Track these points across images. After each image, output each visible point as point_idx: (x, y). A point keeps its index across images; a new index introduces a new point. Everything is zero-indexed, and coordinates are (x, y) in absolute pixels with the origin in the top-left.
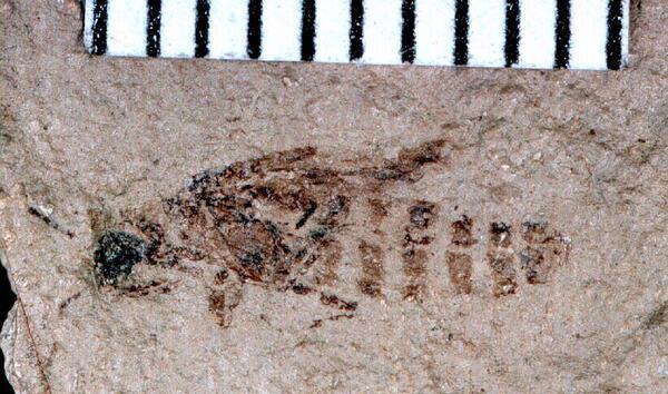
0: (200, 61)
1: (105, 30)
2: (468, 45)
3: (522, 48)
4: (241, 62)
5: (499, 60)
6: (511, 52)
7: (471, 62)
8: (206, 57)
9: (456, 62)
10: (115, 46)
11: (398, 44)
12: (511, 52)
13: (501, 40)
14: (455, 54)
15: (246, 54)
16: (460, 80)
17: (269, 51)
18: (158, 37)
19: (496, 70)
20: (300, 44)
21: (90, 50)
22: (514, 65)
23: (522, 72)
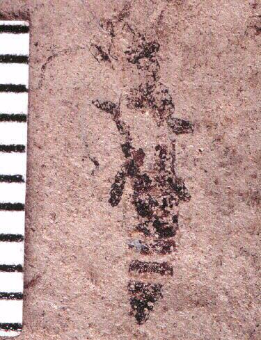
0: (32, 60)
1: (7, 324)
2: (15, 114)
3: (17, 83)
4: (31, 36)
5: (24, 96)
6: (19, 89)
7: (25, 112)
8: (23, 266)
9: (25, 121)
10: (18, 318)
11: (15, 213)
12: (19, 89)
13: (12, 95)
14: (20, 122)
15: (21, 243)
16: (25, 328)
17: (22, 171)
18: (12, 294)
19: (29, 97)
20: (18, 55)
21: (20, 333)
22: (27, 87)
23: (30, 83)
